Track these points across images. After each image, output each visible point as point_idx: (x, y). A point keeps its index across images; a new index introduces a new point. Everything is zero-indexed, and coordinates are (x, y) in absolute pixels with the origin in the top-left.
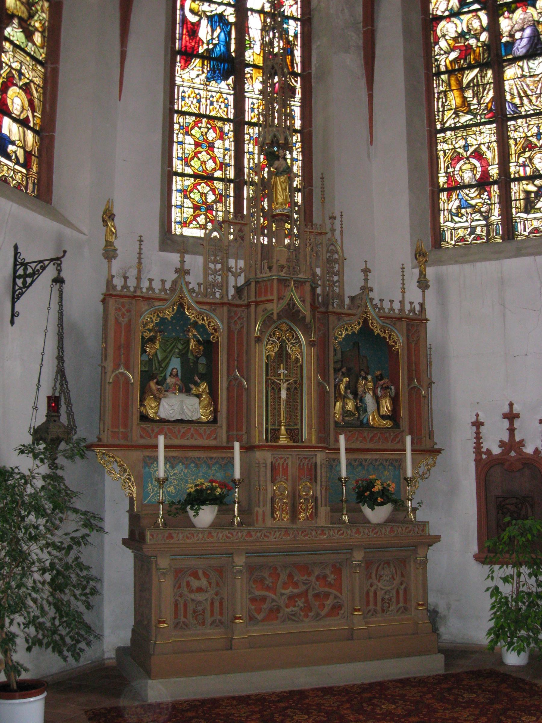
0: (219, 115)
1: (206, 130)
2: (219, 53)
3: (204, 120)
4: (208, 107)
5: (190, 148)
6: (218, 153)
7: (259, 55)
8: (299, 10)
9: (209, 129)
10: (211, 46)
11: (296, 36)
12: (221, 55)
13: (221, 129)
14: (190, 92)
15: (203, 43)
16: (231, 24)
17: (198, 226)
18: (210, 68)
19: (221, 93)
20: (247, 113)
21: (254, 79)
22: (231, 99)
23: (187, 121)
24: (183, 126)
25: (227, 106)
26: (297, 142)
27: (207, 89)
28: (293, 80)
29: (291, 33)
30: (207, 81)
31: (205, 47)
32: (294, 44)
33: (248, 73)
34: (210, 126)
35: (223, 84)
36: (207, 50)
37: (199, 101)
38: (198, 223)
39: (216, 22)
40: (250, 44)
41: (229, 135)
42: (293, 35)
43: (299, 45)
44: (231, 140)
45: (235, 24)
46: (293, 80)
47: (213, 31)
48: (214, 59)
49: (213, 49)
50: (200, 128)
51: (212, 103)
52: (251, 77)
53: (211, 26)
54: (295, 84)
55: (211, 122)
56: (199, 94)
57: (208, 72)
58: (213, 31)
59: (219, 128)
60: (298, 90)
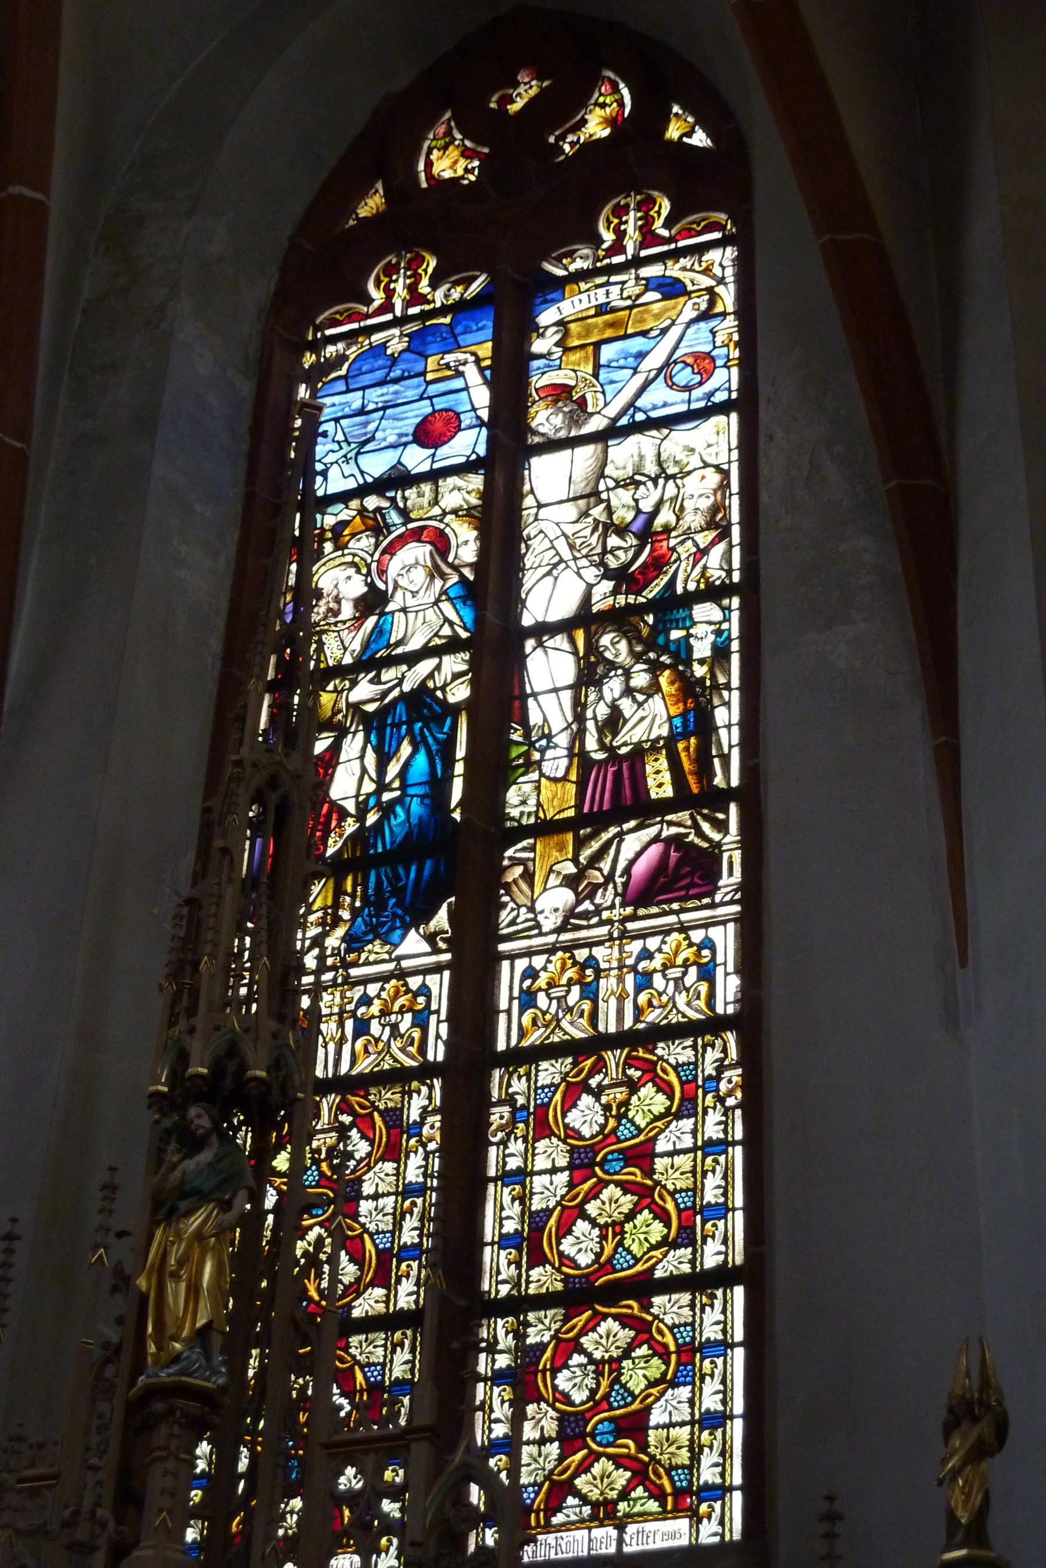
0: (674, 1018)
1: (620, 1094)
2: (400, 832)
3: (612, 1058)
4: (347, 1048)
5: (548, 1190)
6: (671, 1172)
7: (565, 779)
8: (736, 553)
9: (633, 1087)
10: (372, 818)
11: (720, 654)
12: (408, 835)
13: (394, 1117)
14: (554, 967)
15: (343, 814)
16: (454, 710)
17: (587, 1510)
18: (365, 898)
19: (402, 975)
20: (502, 1018)
21: (538, 879)
22: (440, 985)
23: (544, 1079)
24: (525, 1107)
25: (421, 1022)
26: (720, 1069)
27: (347, 977)
28: (706, 827)
29: (702, 649)
30: (348, 951)
31: (350, 826)
32: (716, 687)
33: (515, 862)
34: (346, 1119)
35: (413, 943)
36: (361, 837)
37: (590, 993)
38: (585, 1500)
39: (398, 726)
40: (527, 755)
41: (426, 1130)
42: (707, 653)
43: (735, 682)
44: (432, 1146)
45: (468, 705)
46: (706, 827)
47: (383, 760)
48: (378, 861)
49: (378, 826)
50: (597, 1093)
51: (362, 1028)
52: (528, 877)
53: (378, 750)
54: (716, 836)
55: (353, 1099)
56: (591, 962)
57: (355, 913)
58: (383, 760)
59: (384, 1114)
60: (733, 857)
